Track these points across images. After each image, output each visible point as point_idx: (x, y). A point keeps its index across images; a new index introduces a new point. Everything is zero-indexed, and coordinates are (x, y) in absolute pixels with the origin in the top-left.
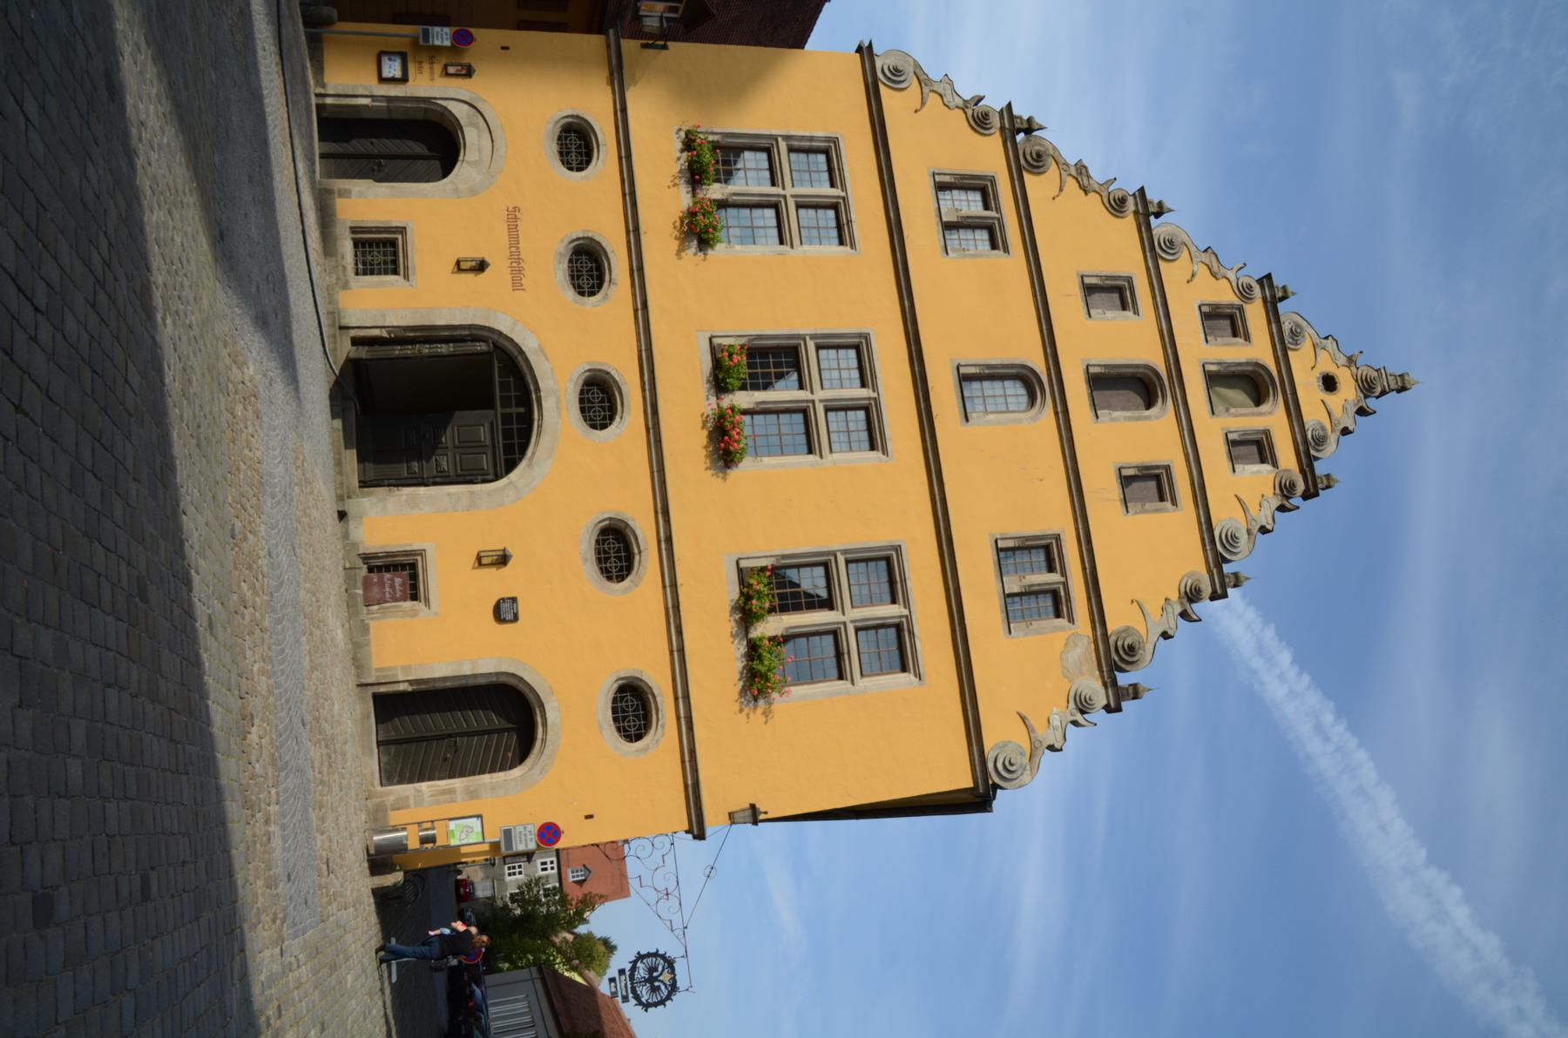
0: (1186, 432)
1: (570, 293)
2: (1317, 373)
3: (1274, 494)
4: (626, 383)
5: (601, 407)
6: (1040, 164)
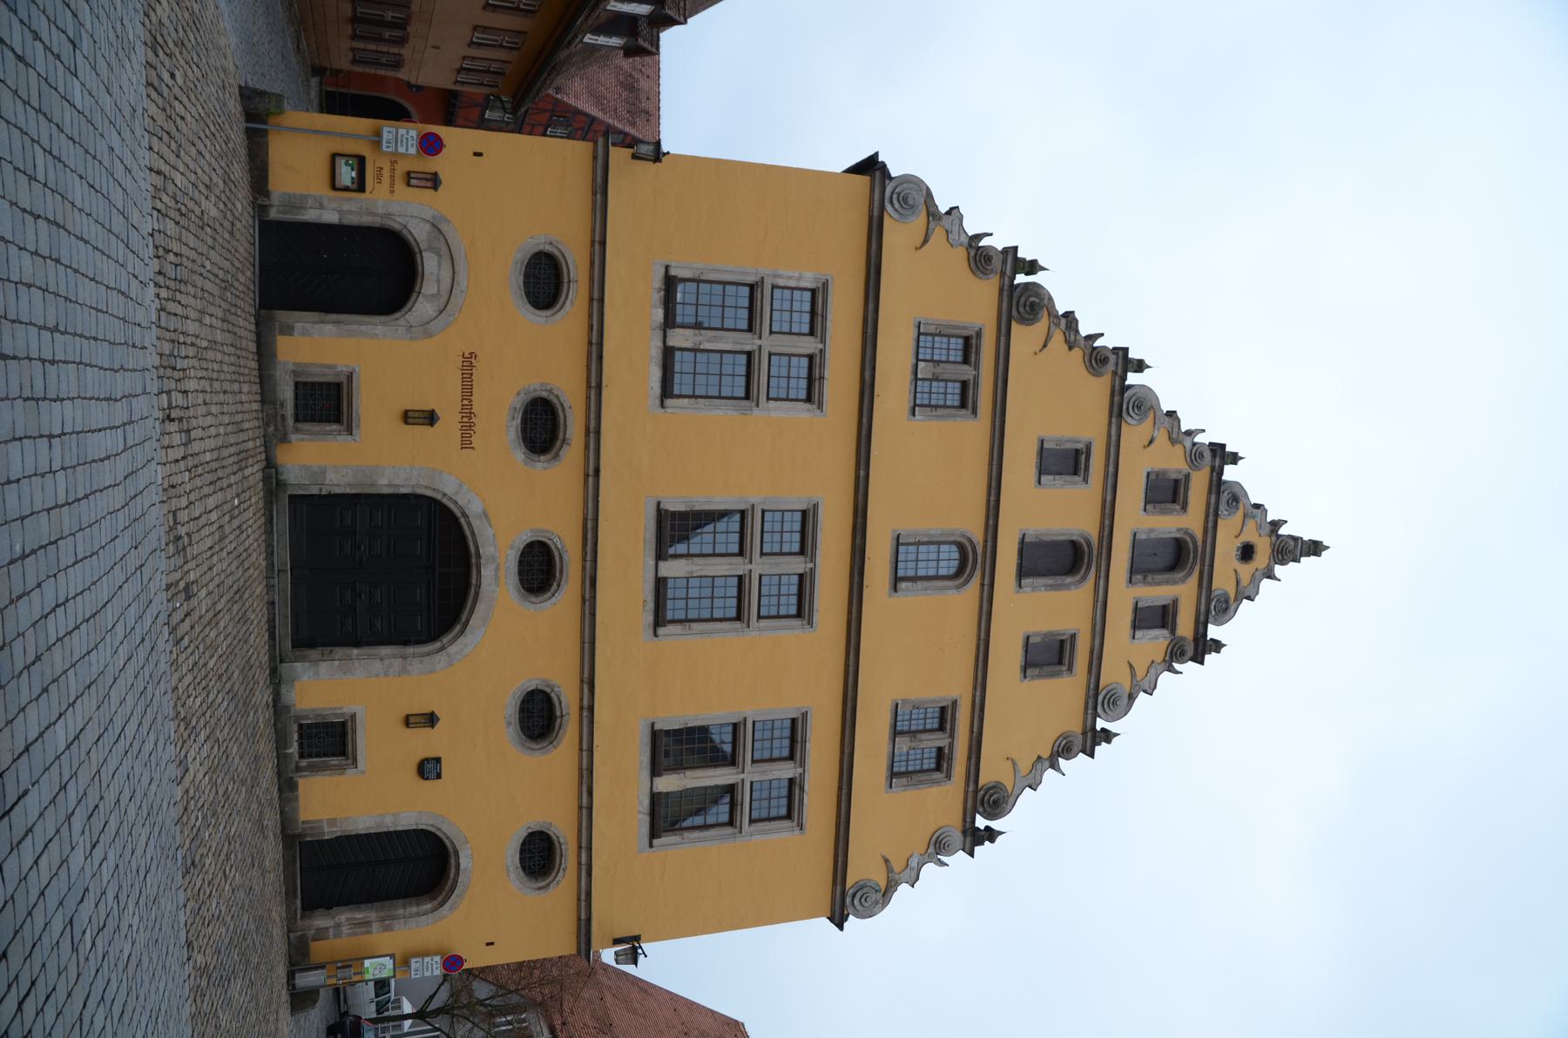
0: (1099, 604)
1: (519, 454)
2: (1238, 543)
3: (1164, 660)
4: (567, 551)
5: (541, 856)
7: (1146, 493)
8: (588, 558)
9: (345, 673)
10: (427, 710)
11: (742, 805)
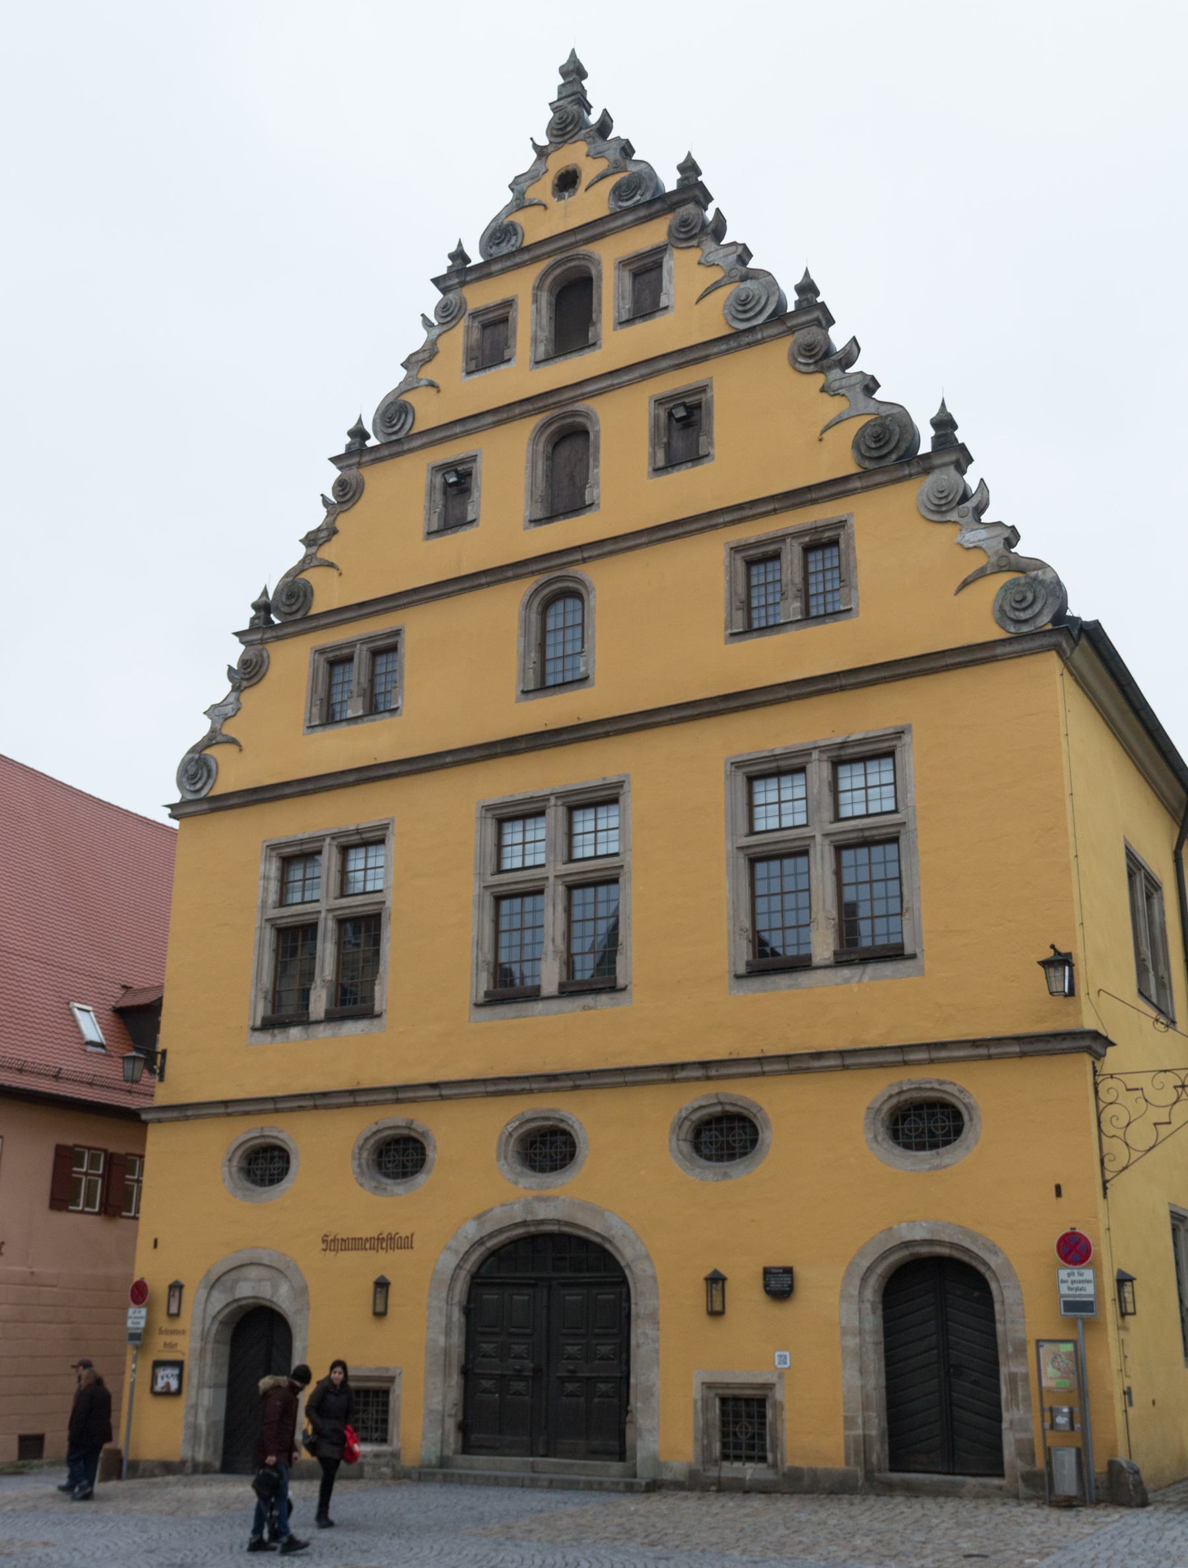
3: (698, 246)
4: (523, 1114)
6: (302, 594)
7: (489, 367)
8: (526, 1086)
9: (652, 1395)
10: (701, 1286)
11: (862, 830)
